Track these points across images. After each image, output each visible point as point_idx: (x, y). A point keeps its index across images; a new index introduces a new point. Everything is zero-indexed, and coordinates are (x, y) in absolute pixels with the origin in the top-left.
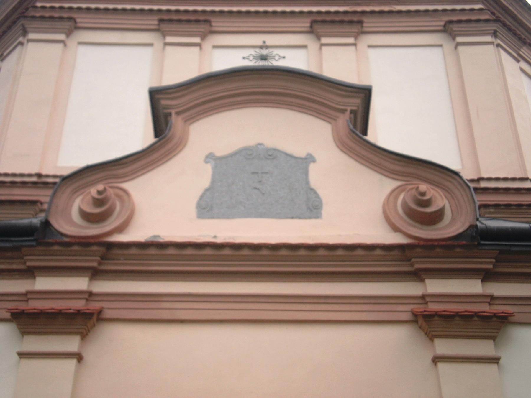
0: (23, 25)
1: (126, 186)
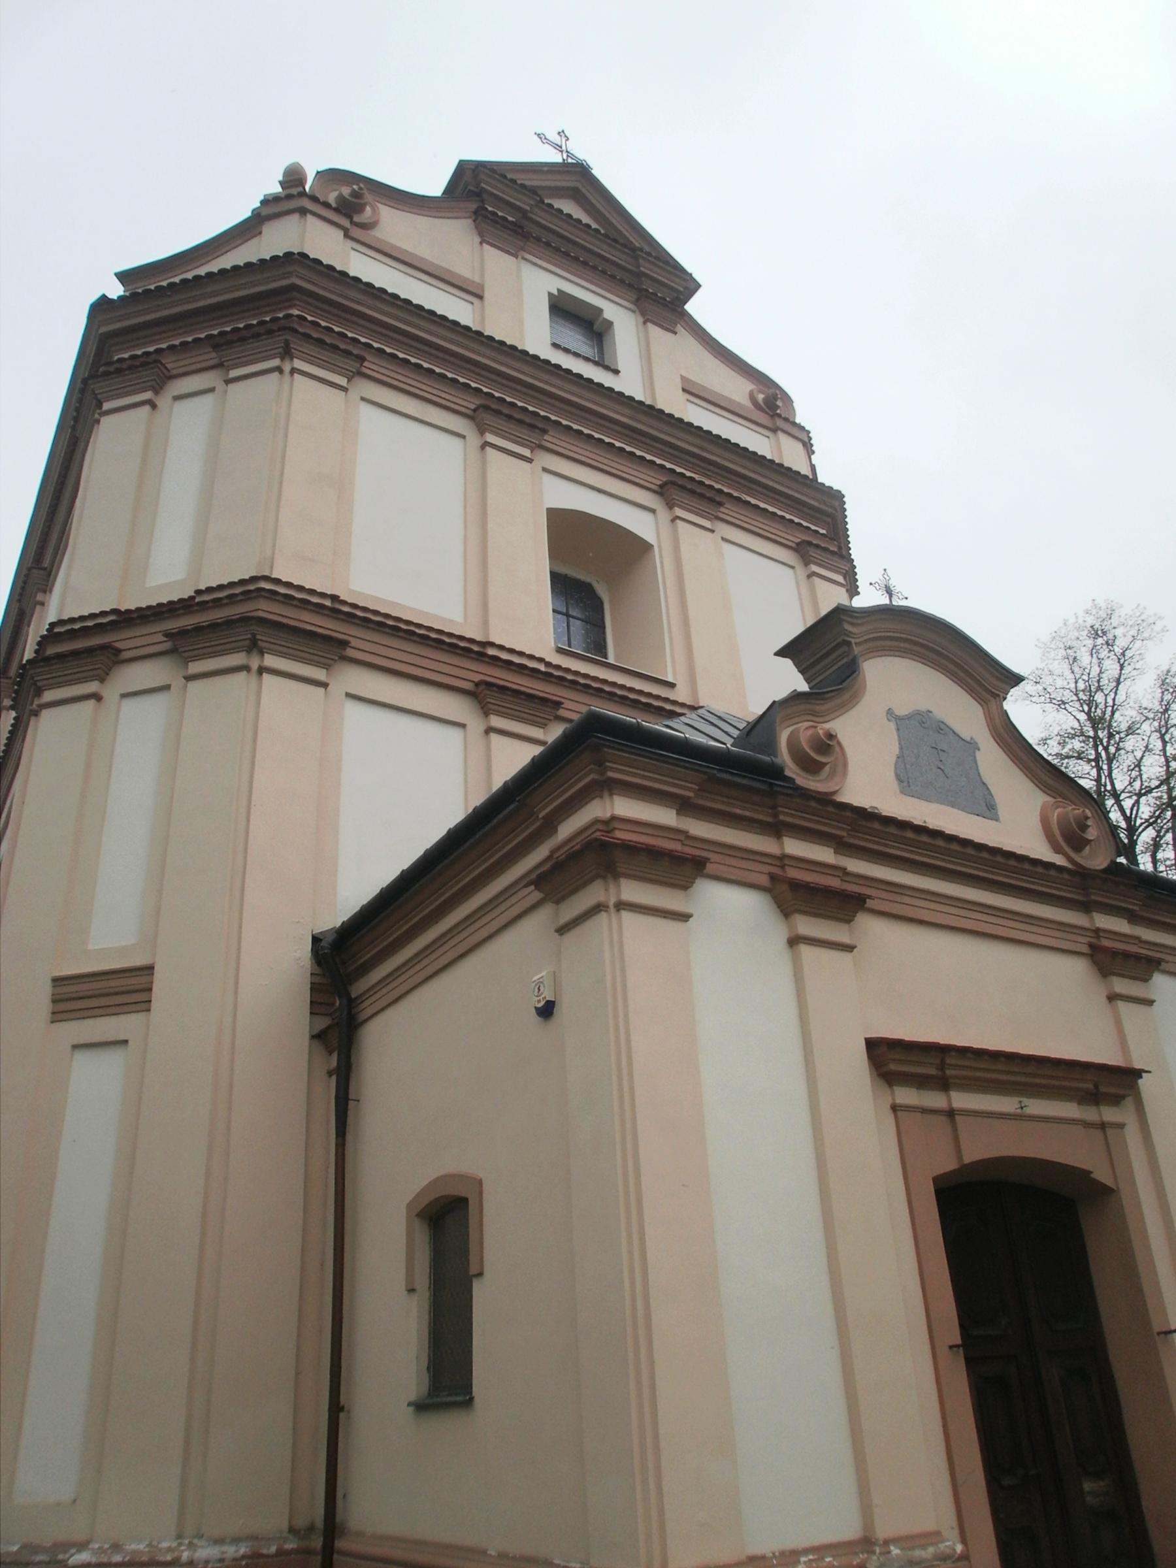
0: (287, 343)
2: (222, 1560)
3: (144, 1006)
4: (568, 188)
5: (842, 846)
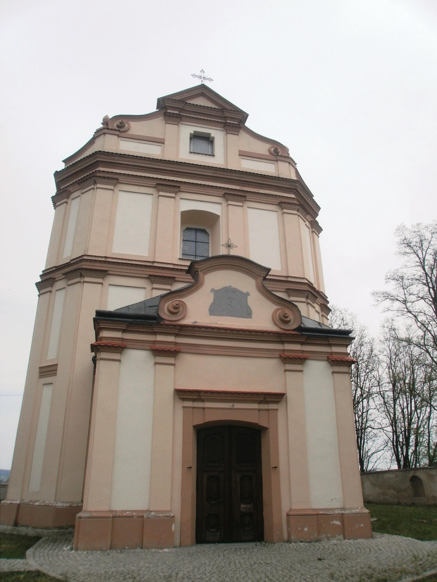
0: (95, 180)
1: (183, 300)
2: (62, 506)
3: (55, 374)
4: (200, 93)
5: (177, 335)
